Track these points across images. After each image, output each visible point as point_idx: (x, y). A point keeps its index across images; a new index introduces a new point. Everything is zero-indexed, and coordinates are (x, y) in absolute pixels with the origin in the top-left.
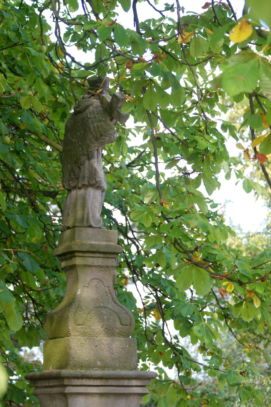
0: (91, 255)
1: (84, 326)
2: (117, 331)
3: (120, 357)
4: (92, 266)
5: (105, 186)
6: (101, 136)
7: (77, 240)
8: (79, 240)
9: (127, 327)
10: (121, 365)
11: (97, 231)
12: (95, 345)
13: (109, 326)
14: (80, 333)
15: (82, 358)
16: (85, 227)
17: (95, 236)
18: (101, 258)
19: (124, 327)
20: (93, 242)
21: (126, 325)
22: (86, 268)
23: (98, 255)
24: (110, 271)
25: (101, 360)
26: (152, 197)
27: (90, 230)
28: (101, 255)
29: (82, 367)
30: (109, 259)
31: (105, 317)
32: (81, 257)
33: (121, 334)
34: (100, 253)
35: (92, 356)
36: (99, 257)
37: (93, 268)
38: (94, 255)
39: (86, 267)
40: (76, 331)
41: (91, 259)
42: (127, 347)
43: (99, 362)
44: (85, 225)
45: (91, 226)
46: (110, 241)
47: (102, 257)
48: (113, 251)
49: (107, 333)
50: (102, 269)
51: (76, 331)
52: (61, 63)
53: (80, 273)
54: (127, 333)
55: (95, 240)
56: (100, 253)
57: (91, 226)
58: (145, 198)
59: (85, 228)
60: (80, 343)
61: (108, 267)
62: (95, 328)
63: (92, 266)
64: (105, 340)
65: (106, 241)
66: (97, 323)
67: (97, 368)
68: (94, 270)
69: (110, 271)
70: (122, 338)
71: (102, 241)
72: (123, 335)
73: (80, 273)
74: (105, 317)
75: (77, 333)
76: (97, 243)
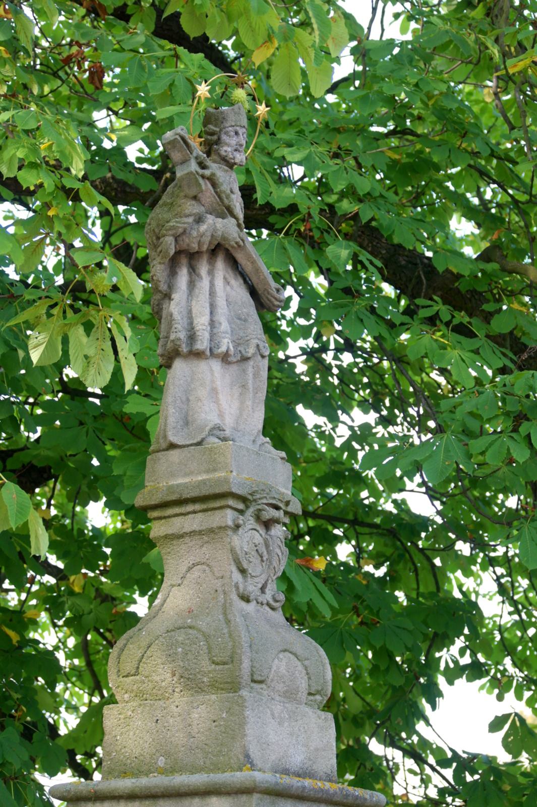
0: (177, 510)
1: (138, 677)
2: (205, 680)
3: (207, 742)
4: (182, 536)
5: (184, 346)
6: (158, 238)
7: (149, 482)
8: (153, 481)
9: (226, 666)
10: (208, 762)
11: (190, 452)
12: (155, 719)
13: (187, 670)
14: (132, 695)
15: (126, 752)
16: (164, 450)
17: (185, 465)
18: (200, 514)
19: (218, 667)
20: (181, 481)
21: (224, 664)
22: (175, 542)
23: (190, 508)
24: (222, 538)
25: (167, 755)
26: (45, 345)
27: (174, 455)
28: (197, 507)
29: (125, 773)
30: (217, 512)
31: (180, 650)
32: (160, 518)
33: (215, 686)
34: (194, 500)
35: (147, 745)
36: (194, 512)
37: (187, 539)
38: (183, 509)
39: (172, 540)
40: (123, 691)
41: (178, 521)
42: (224, 715)
43: (161, 758)
44: (164, 446)
45: (172, 446)
46: (215, 470)
47: (200, 511)
48: (218, 491)
49: (187, 687)
50: (206, 538)
51: (123, 691)
52: (87, 121)
53: (165, 557)
54: (227, 683)
55: (186, 475)
56: (194, 500)
57: (172, 446)
58: (31, 352)
59: (166, 452)
60: (122, 716)
61: (211, 531)
62: (158, 678)
63: (182, 536)
64: (179, 701)
65: (208, 471)
66: (162, 666)
67: (156, 774)
68: (191, 544)
69: (222, 538)
70: (214, 697)
71: (199, 473)
72: (222, 689)
73: (165, 557)
74: (180, 650)
75: (126, 696)
76: (187, 480)
